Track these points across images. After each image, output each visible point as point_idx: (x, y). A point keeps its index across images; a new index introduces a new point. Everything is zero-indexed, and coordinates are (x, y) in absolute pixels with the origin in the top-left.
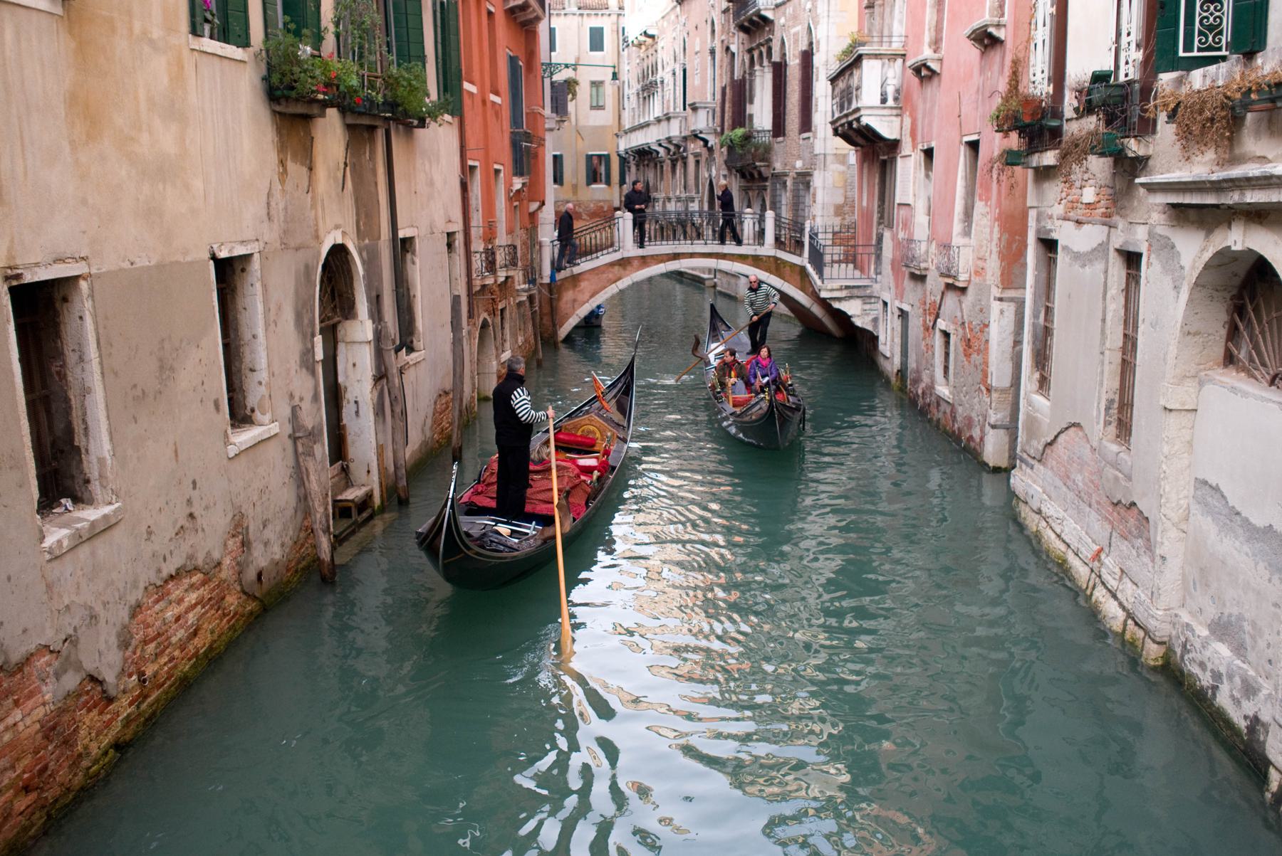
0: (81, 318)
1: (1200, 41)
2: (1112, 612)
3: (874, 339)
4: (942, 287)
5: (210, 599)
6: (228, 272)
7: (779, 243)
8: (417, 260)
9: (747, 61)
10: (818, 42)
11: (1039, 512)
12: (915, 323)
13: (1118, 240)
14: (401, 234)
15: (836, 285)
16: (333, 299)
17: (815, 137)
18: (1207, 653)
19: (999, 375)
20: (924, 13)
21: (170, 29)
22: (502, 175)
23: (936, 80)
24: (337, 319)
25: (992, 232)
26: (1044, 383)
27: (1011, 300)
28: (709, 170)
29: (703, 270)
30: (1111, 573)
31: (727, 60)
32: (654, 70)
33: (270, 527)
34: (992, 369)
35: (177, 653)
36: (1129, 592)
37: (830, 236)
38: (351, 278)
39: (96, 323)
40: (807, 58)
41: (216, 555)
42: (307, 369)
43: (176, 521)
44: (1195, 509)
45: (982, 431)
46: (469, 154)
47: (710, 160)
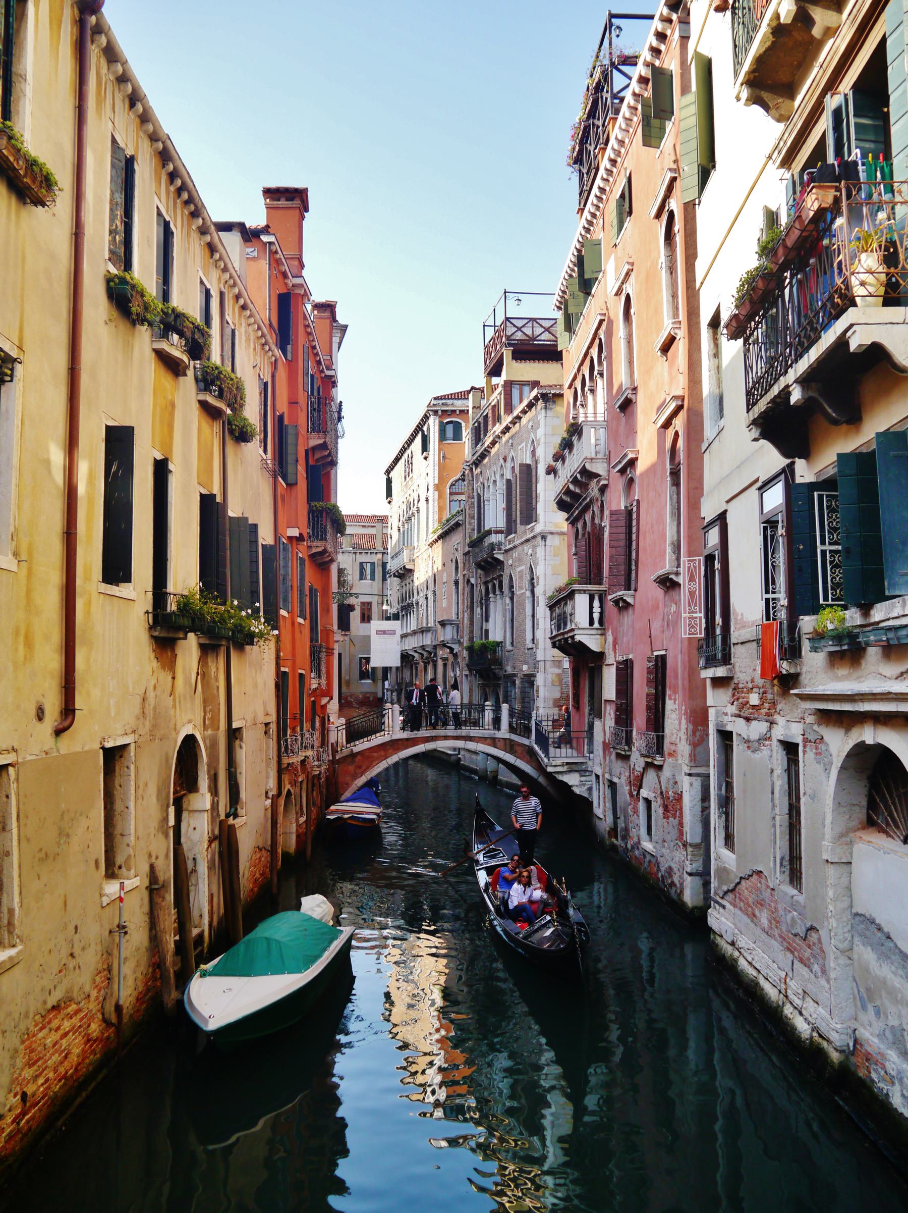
0: (7, 797)
2: (802, 1027)
4: (643, 765)
5: (80, 1027)
7: (512, 729)
8: (244, 745)
9: (483, 590)
10: (538, 578)
12: (624, 790)
13: (779, 732)
15: (559, 761)
19: (692, 832)
23: (630, 610)
25: (680, 723)
27: (698, 775)
29: (450, 748)
31: (467, 590)
34: (687, 828)
35: (51, 1075)
36: (812, 1010)
37: (550, 723)
39: (18, 801)
41: (87, 988)
43: (61, 960)
47: (455, 664)
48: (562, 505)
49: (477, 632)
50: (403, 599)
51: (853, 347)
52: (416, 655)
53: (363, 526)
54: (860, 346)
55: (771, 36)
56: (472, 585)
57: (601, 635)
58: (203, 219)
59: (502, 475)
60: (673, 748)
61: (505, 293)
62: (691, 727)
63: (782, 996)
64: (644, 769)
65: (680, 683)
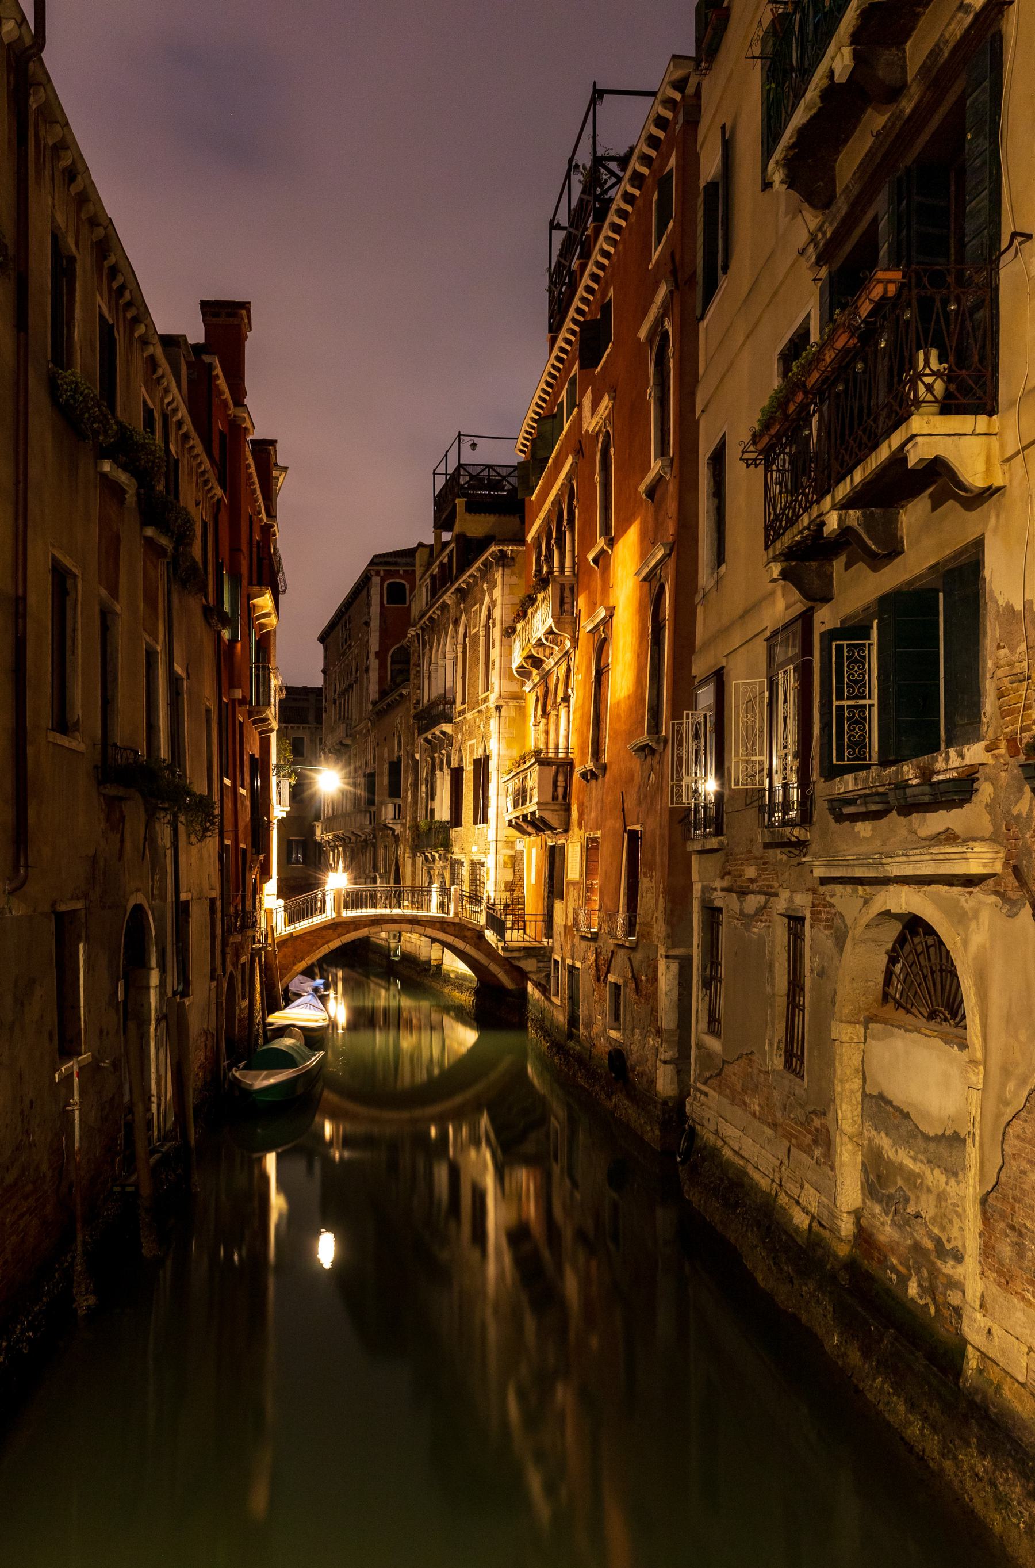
1: (849, 753)
14: (183, 897)
19: (668, 1020)
25: (657, 902)
27: (675, 957)
49: (421, 812)
51: (912, 461)
54: (922, 460)
55: (818, 100)
58: (146, 326)
61: (460, 435)
62: (669, 905)
65: (658, 859)
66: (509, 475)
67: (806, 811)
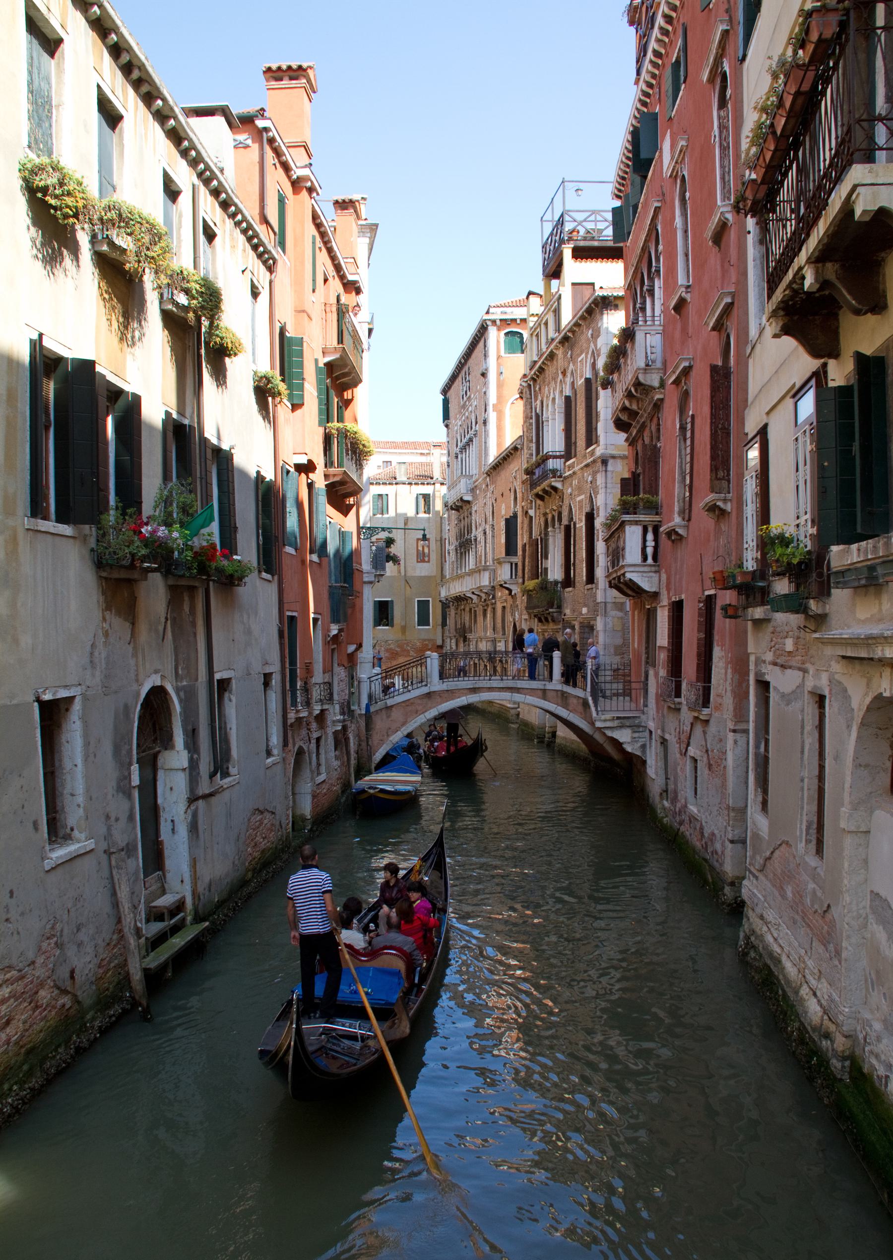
3: (644, 762)
6: (52, 713)
8: (233, 698)
10: (598, 508)
11: (762, 917)
12: (674, 749)
13: (810, 684)
14: (217, 676)
15: (608, 716)
16: (155, 732)
17: (597, 588)
18: (882, 1046)
20: (674, 486)
21: (9, 512)
22: (320, 622)
24: (158, 749)
26: (765, 804)
28: (513, 614)
30: (812, 974)
31: (526, 521)
32: (469, 531)
33: (83, 930)
38: (170, 715)
40: (590, 518)
42: (124, 793)
44: (871, 919)
45: (723, 845)
46: (286, 606)
47: (514, 607)
48: (620, 425)
50: (460, 535)
52: (474, 597)
53: (422, 454)
56: (531, 518)
57: (655, 572)
59: (561, 392)
60: (719, 700)
62: (737, 677)
63: (800, 976)
64: (692, 724)
66: (585, 220)
67: (823, 582)
